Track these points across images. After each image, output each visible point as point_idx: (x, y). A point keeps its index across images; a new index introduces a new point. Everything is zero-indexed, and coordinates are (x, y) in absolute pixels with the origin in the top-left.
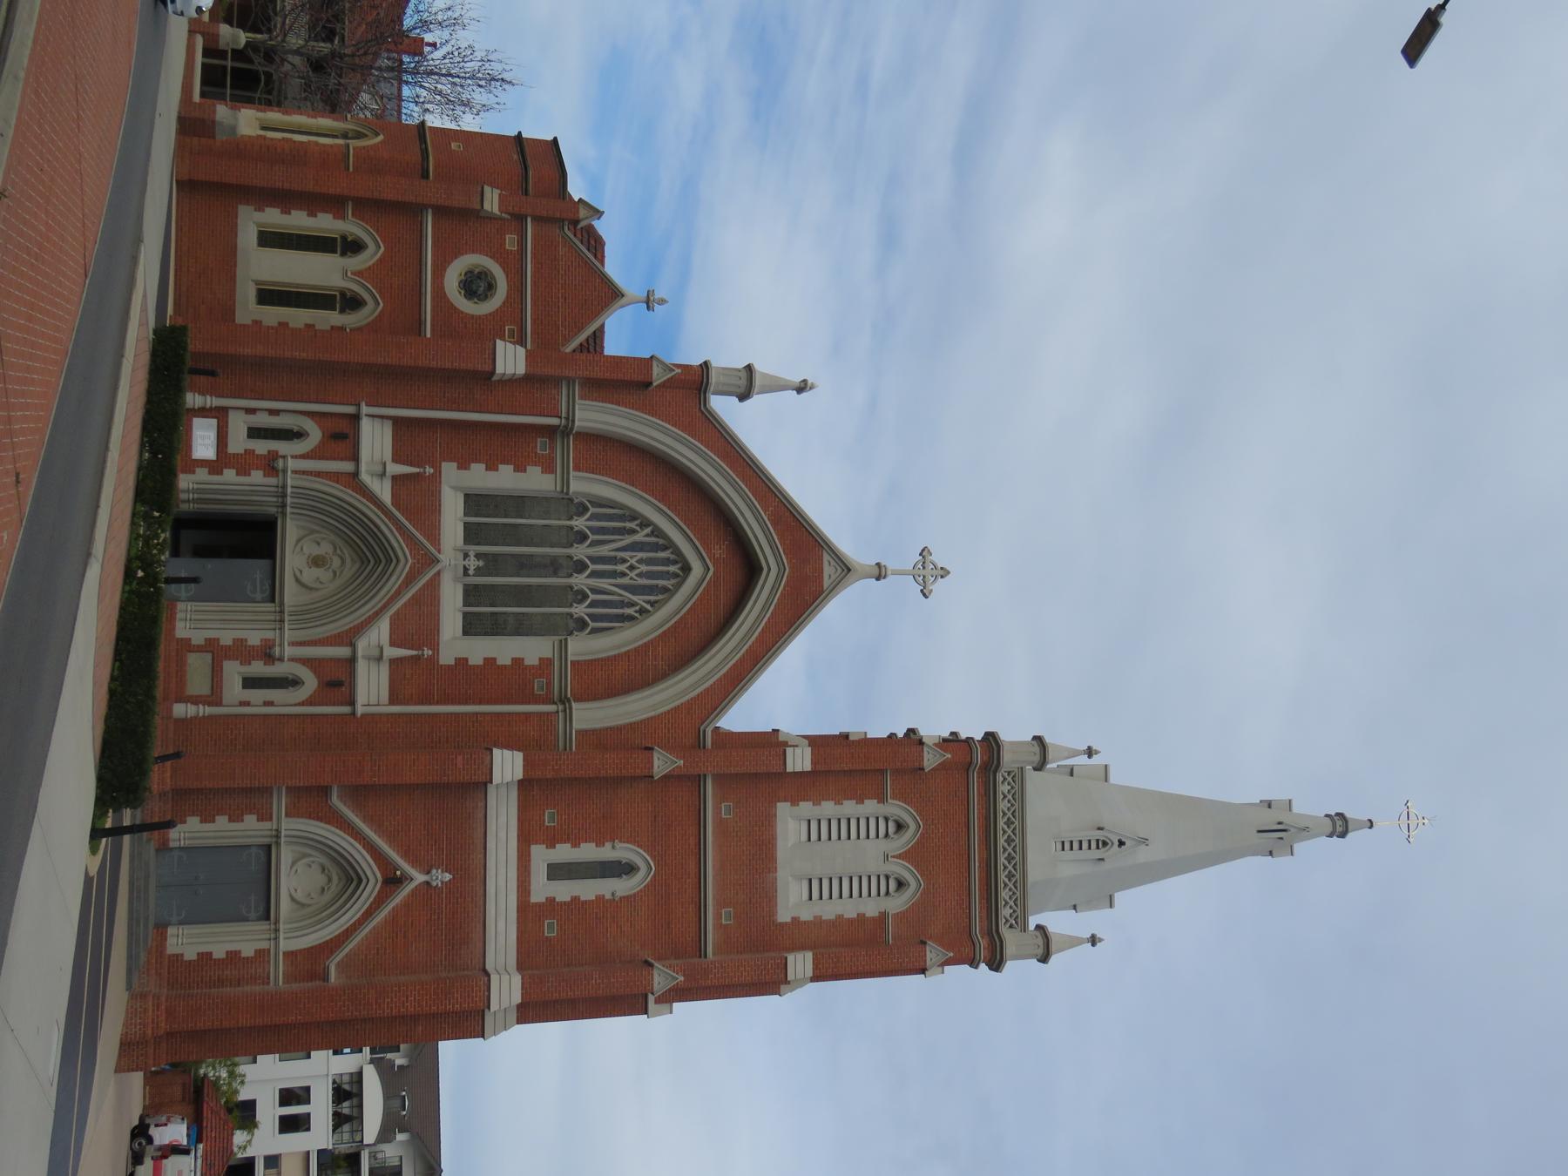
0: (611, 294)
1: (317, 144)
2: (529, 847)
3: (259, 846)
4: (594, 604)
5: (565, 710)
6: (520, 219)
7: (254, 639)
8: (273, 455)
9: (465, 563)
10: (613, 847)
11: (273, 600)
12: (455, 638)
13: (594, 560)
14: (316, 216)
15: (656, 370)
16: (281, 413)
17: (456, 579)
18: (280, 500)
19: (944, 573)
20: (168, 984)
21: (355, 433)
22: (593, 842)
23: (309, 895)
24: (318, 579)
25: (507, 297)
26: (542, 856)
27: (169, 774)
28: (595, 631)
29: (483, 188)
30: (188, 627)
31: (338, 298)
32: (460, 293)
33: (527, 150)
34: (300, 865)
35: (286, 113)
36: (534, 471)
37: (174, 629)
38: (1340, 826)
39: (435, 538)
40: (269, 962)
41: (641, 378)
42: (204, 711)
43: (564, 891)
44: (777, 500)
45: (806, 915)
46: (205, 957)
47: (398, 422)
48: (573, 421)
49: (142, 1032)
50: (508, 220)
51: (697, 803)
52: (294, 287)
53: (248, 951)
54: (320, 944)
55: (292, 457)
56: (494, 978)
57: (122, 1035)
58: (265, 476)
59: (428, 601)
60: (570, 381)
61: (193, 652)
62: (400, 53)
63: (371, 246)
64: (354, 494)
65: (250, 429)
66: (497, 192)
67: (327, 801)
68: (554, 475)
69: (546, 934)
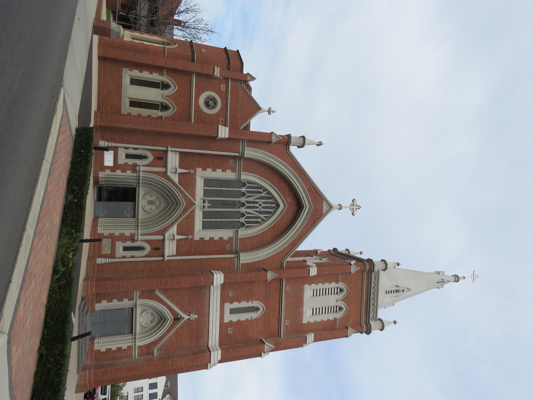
0: (256, 108)
1: (153, 46)
2: (224, 304)
3: (129, 308)
4: (247, 218)
5: (237, 257)
6: (226, 79)
7: (127, 233)
8: (135, 165)
9: (204, 204)
10: (252, 302)
11: (135, 217)
12: (199, 231)
13: (248, 202)
14: (152, 74)
15: (273, 137)
16: (138, 149)
17: (200, 209)
18: (137, 181)
19: (359, 207)
20: (95, 361)
21: (165, 157)
22: (245, 301)
23: (147, 323)
24: (151, 209)
25: (221, 108)
26: (228, 306)
27: (94, 288)
28: (247, 227)
29: (214, 67)
30: (102, 229)
31: (160, 105)
32: (204, 106)
33: (229, 54)
34: (144, 314)
35: (142, 34)
36: (229, 172)
37: (97, 230)
38: (457, 278)
39: (194, 196)
40: (132, 350)
41: (268, 140)
42: (110, 260)
43: (235, 318)
44: (310, 183)
45: (312, 321)
46: (109, 350)
47: (181, 153)
48: (244, 155)
49: (84, 383)
50: (222, 79)
51: (280, 286)
52: (143, 101)
53: (124, 347)
54: (151, 343)
55: (142, 166)
56: (212, 353)
57: (77, 385)
58: (132, 173)
59: (191, 218)
60: (243, 140)
61: (104, 238)
62: (173, 25)
63: (173, 87)
64: (165, 180)
65: (126, 155)
66: (219, 68)
67: (154, 292)
68: (235, 173)
69: (229, 333)
